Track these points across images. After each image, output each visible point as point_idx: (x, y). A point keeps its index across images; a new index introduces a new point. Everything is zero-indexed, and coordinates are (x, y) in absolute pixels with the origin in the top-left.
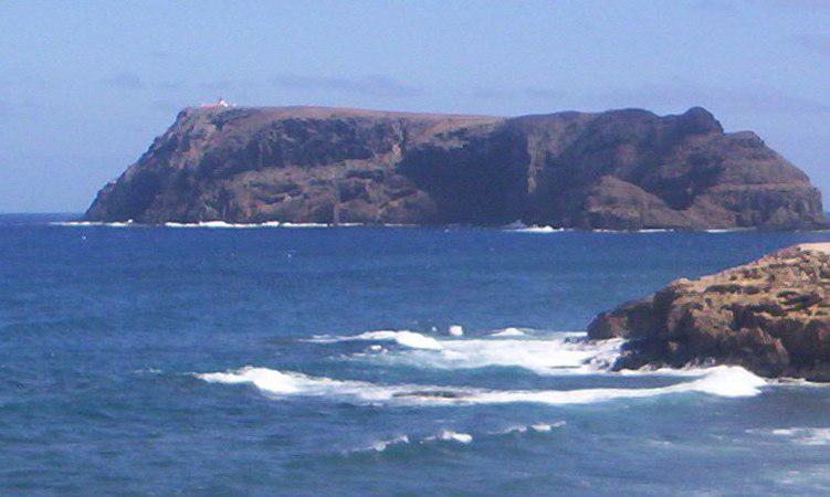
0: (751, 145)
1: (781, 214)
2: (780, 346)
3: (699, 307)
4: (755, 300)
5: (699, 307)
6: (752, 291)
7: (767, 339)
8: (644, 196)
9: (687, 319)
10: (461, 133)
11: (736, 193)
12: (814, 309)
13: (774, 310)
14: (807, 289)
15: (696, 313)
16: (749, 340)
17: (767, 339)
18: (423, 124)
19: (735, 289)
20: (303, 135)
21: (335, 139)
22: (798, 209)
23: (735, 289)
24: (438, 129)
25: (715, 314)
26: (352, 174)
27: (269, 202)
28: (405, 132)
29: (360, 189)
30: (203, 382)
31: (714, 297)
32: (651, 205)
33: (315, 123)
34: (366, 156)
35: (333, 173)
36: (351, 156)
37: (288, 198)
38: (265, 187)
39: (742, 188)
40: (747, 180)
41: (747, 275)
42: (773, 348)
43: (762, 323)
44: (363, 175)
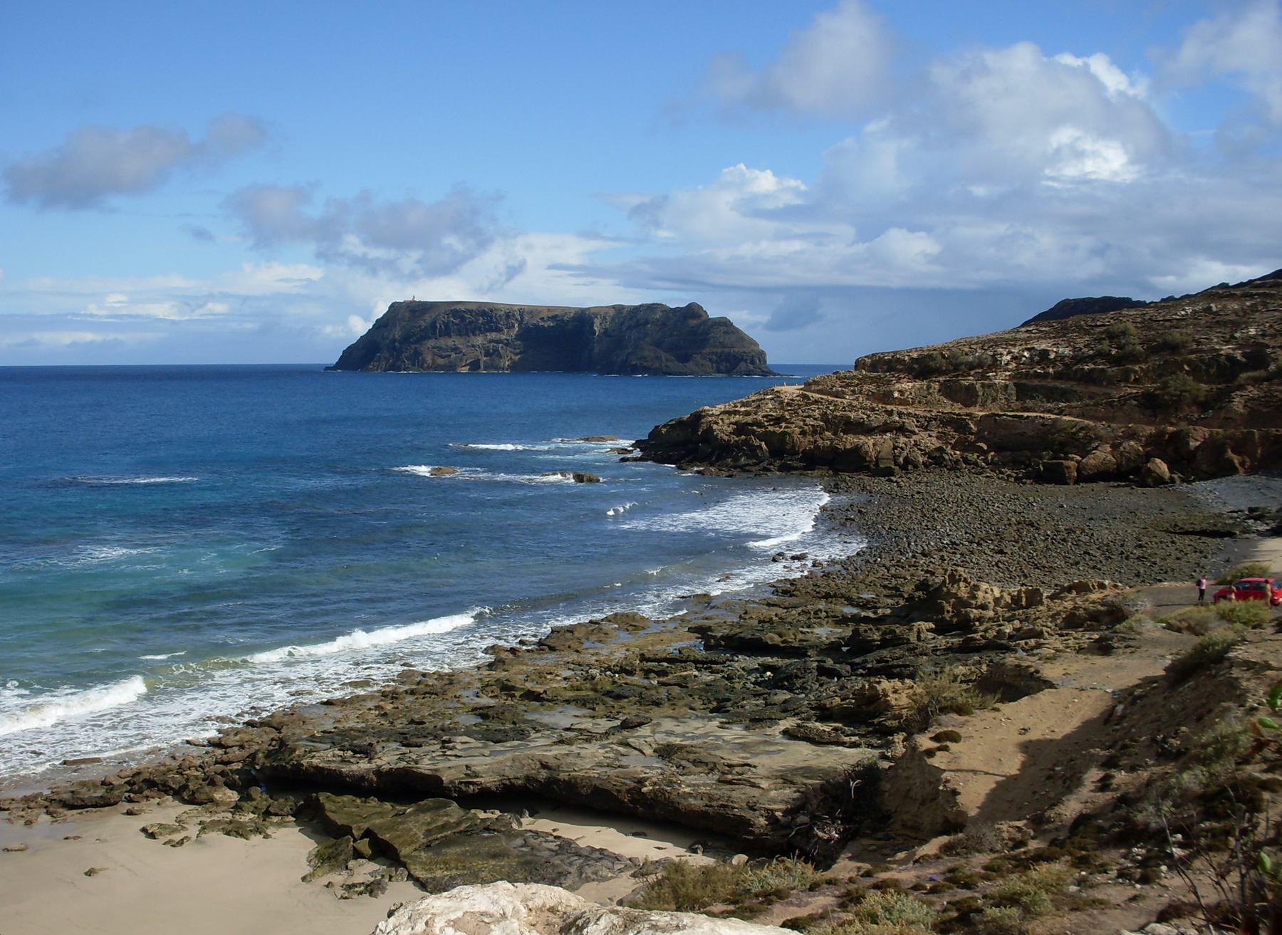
0: (724, 323)
1: (743, 366)
2: (764, 447)
3: (717, 423)
4: (749, 419)
5: (717, 423)
6: (747, 414)
7: (757, 443)
8: (663, 355)
9: (710, 430)
10: (554, 318)
11: (716, 354)
12: (783, 425)
13: (760, 425)
14: (779, 413)
15: (715, 427)
16: (746, 442)
17: (757, 443)
18: (533, 311)
19: (736, 413)
20: (463, 319)
21: (481, 320)
22: (753, 362)
23: (736, 413)
24: (544, 315)
25: (725, 427)
26: (491, 341)
27: (442, 357)
28: (521, 315)
29: (496, 350)
30: (142, 662)
31: (725, 417)
32: (667, 360)
33: (470, 312)
34: (499, 330)
35: (479, 340)
36: (491, 330)
37: (454, 355)
38: (440, 348)
39: (719, 350)
40: (723, 345)
41: (743, 405)
42: (760, 446)
43: (754, 433)
44: (497, 342)
